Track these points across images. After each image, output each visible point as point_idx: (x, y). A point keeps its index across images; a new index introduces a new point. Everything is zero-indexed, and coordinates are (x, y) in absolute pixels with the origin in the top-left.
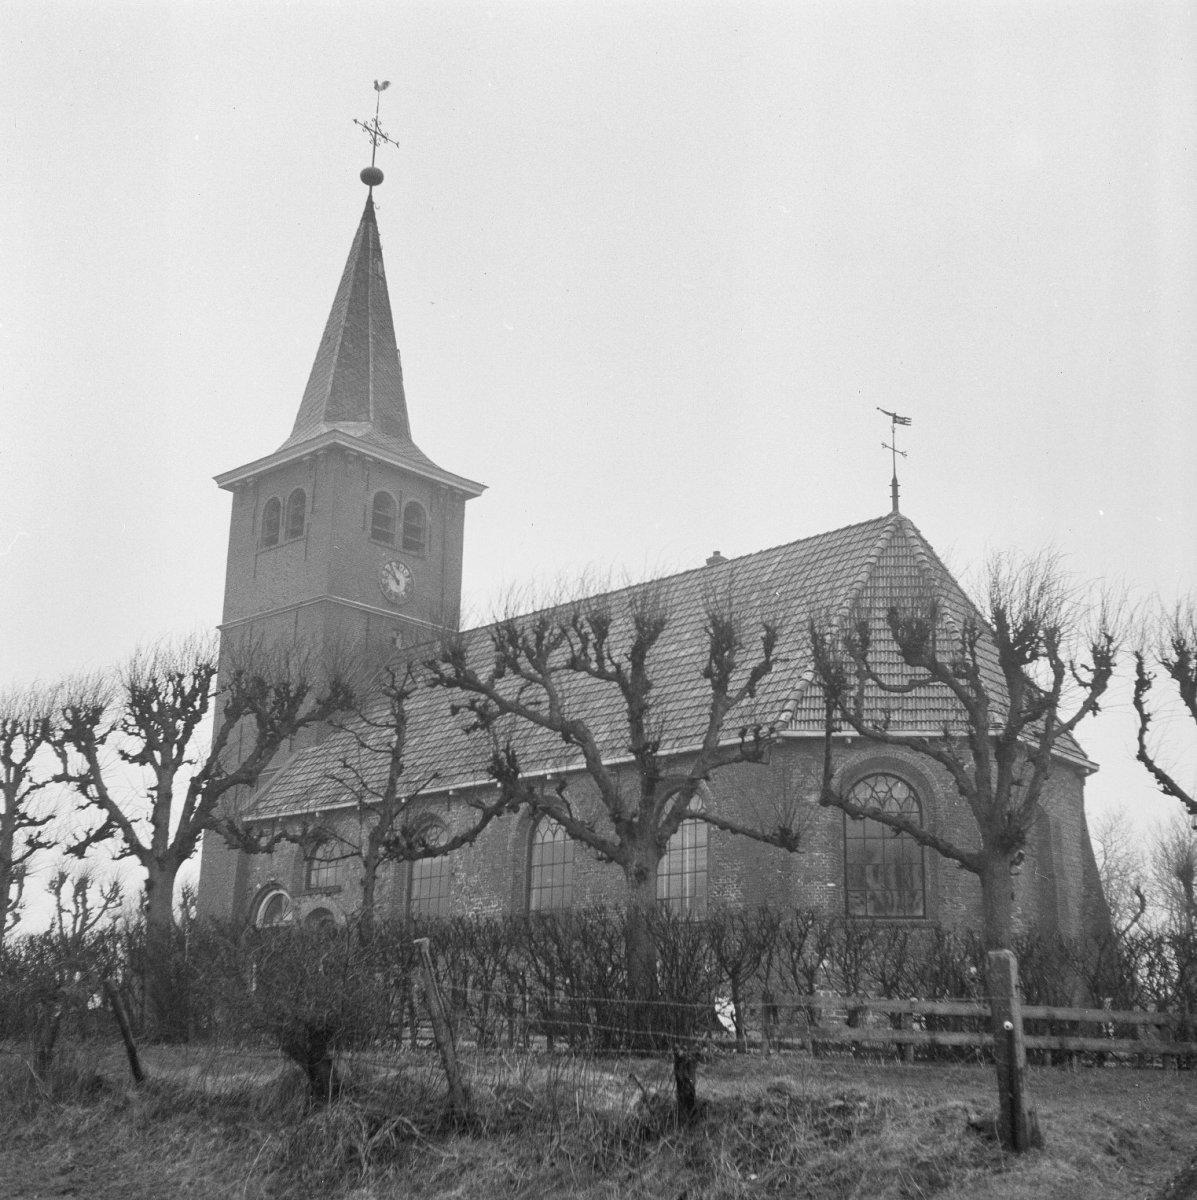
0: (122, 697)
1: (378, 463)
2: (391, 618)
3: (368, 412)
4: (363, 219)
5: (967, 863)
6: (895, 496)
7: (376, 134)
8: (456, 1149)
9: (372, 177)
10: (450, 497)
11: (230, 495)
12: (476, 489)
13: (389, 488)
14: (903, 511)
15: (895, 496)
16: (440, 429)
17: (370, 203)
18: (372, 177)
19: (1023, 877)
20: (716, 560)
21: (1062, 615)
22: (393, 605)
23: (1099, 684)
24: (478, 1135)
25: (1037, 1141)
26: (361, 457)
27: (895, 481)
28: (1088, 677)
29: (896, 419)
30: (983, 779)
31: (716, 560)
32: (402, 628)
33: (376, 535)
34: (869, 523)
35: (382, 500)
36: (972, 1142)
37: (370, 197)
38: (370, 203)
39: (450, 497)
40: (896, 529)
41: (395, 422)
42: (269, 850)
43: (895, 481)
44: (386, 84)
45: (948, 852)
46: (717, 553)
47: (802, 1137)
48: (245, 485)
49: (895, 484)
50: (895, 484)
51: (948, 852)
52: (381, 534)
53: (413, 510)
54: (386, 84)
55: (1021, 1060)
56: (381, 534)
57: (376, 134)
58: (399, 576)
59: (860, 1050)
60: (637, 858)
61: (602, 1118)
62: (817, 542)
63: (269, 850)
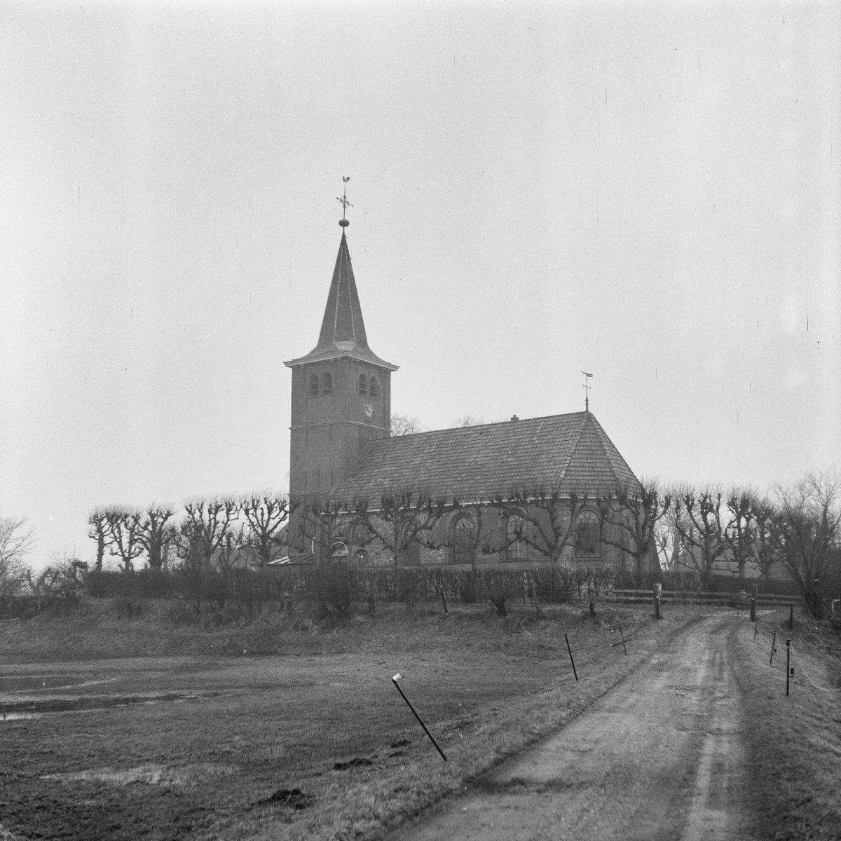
0: (378, 501)
1: (361, 362)
2: (368, 427)
3: (353, 337)
4: (341, 244)
5: (633, 555)
6: (587, 405)
7: (345, 202)
8: (542, 623)
9: (344, 224)
10: (385, 371)
11: (291, 370)
12: (397, 367)
13: (362, 371)
14: (590, 410)
15: (587, 405)
16: (382, 341)
17: (344, 236)
18: (344, 224)
19: (647, 559)
20: (515, 419)
21: (658, 490)
22: (367, 421)
23: (666, 507)
24: (546, 620)
25: (662, 618)
26: (355, 361)
27: (587, 399)
28: (664, 504)
29: (588, 375)
30: (638, 534)
31: (515, 419)
32: (371, 430)
33: (361, 392)
34: (577, 413)
35: (362, 377)
36: (650, 618)
37: (344, 233)
38: (344, 236)
39: (385, 371)
40: (586, 419)
41: (362, 342)
42: (438, 549)
43: (587, 399)
44: (348, 178)
45: (629, 552)
46: (515, 416)
47: (618, 618)
48: (299, 368)
49: (587, 400)
50: (587, 400)
51: (629, 552)
52: (363, 392)
53: (373, 379)
54: (348, 178)
55: (659, 603)
56: (363, 392)
57: (345, 202)
58: (370, 409)
59: (607, 601)
60: (554, 555)
61: (574, 616)
62: (557, 418)
63: (438, 549)
